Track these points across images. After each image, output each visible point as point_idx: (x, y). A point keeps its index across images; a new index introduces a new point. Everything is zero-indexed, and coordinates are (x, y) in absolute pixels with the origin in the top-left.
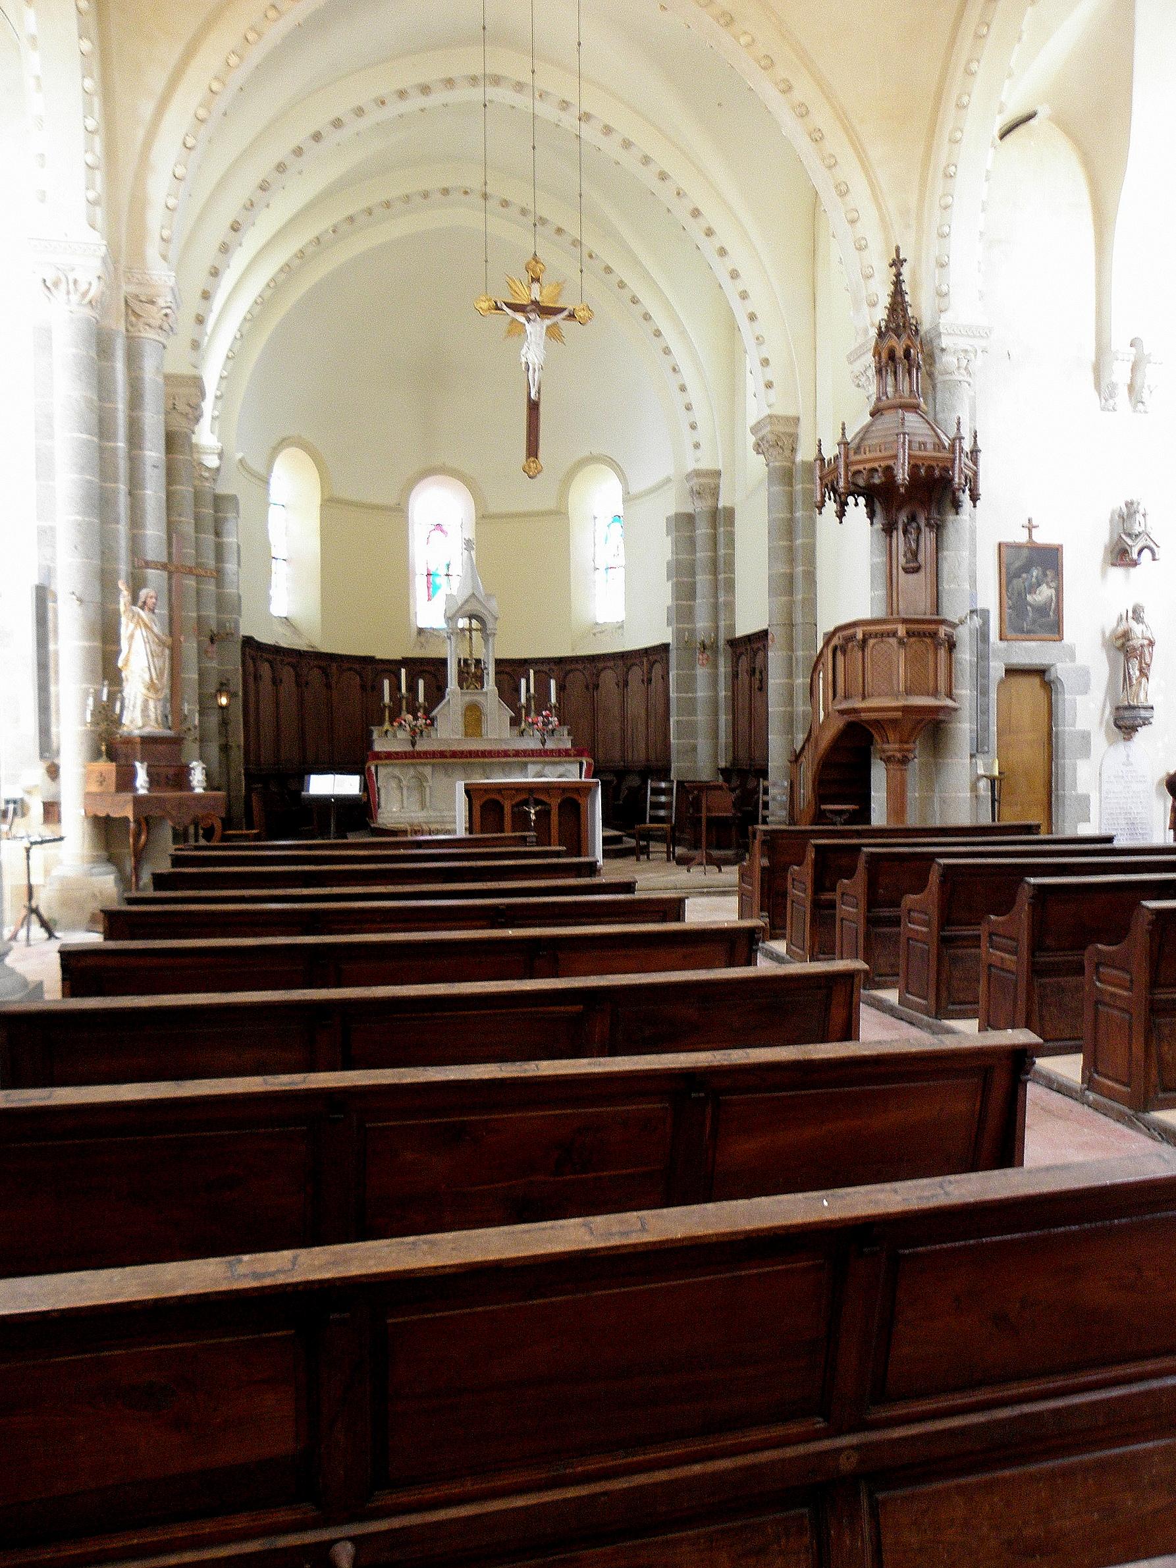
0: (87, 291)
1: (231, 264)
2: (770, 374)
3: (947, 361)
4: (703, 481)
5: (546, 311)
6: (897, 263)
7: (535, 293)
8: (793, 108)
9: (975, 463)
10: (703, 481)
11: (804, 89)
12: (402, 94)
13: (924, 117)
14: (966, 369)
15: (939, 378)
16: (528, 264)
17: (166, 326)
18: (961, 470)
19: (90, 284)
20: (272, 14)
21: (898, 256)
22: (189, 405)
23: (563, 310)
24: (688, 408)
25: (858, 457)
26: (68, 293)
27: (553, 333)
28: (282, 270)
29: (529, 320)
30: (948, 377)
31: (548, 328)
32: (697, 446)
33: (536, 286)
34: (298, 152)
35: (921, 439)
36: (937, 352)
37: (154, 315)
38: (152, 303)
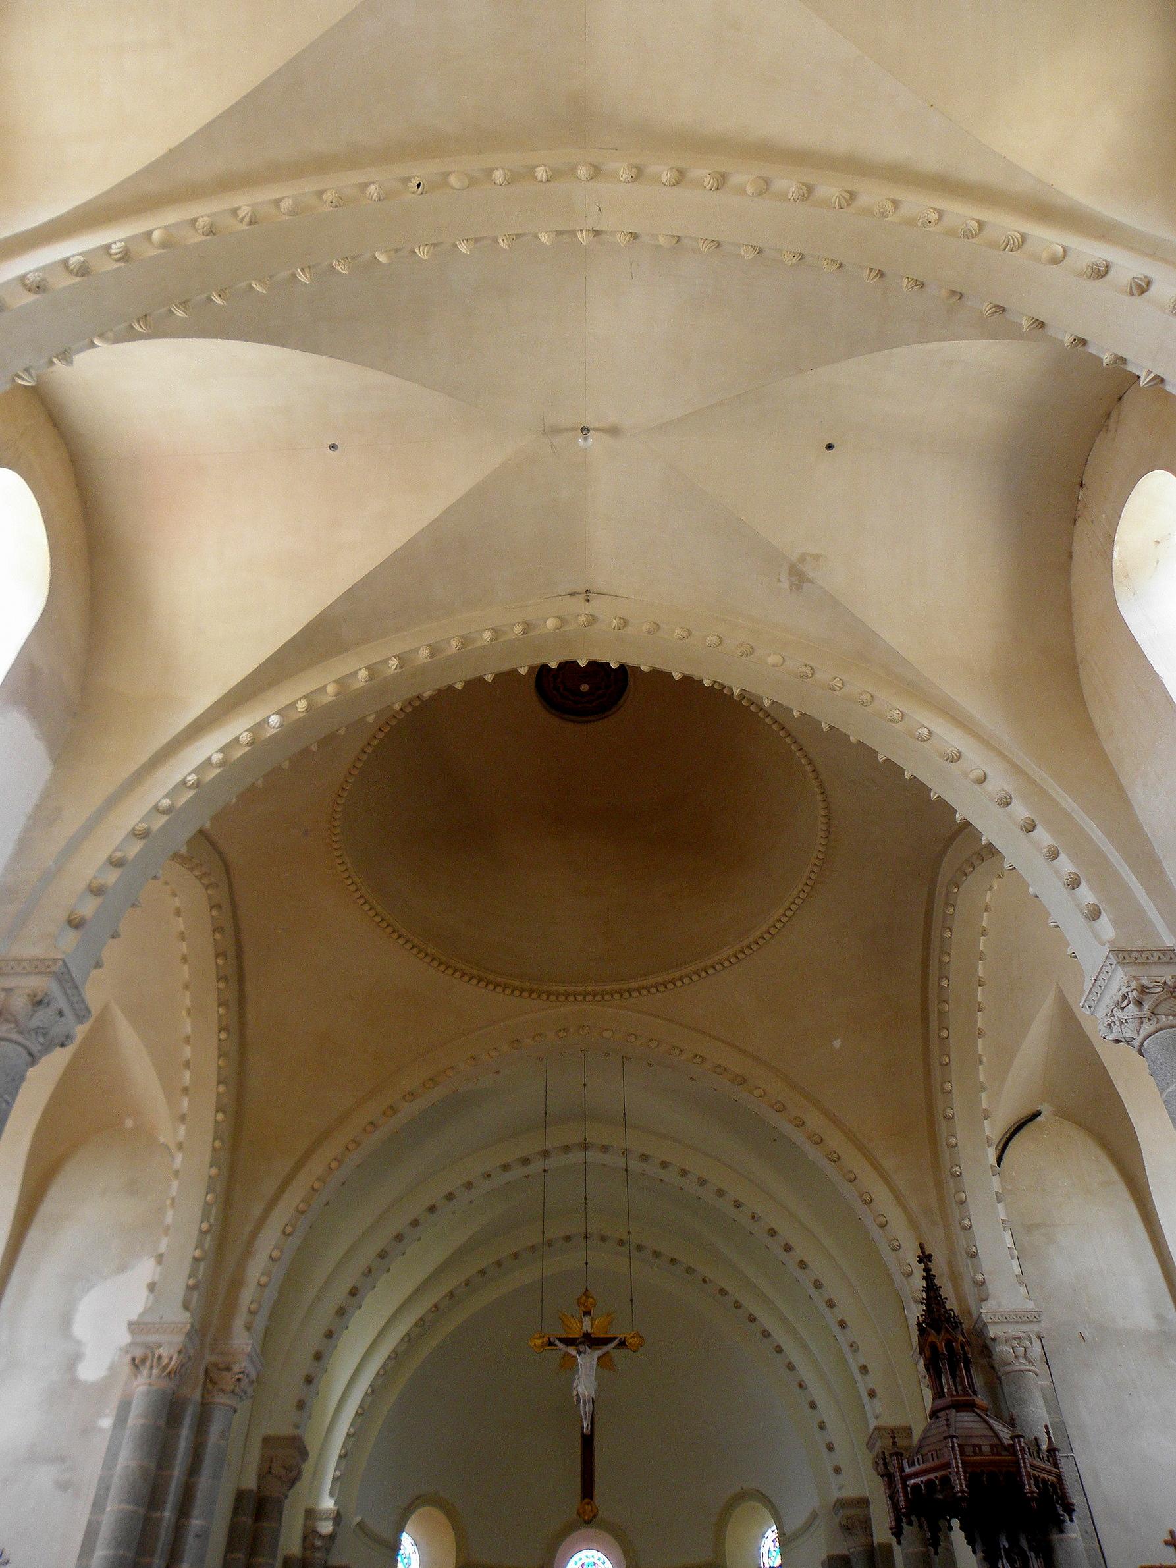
0: (169, 1364)
1: (350, 1324)
2: (871, 1381)
3: (1003, 1350)
4: (850, 1512)
5: (592, 1341)
6: (925, 1258)
7: (587, 1325)
8: (809, 1138)
9: (1056, 1465)
10: (850, 1512)
11: (815, 1121)
12: (506, 1167)
13: (921, 1126)
14: (1025, 1357)
15: (1002, 1370)
16: (580, 1298)
17: (237, 1390)
18: (1028, 1474)
19: (171, 1358)
20: (369, 1128)
21: (923, 1252)
22: (284, 1467)
23: (615, 1338)
24: (822, 1427)
25: (913, 1469)
26: (152, 1367)
27: (604, 1363)
28: (416, 1324)
29: (580, 1353)
30: (1008, 1368)
31: (599, 1358)
32: (837, 1470)
33: (587, 1318)
34: (415, 1223)
35: (975, 1441)
36: (989, 1342)
37: (228, 1381)
38: (228, 1369)
